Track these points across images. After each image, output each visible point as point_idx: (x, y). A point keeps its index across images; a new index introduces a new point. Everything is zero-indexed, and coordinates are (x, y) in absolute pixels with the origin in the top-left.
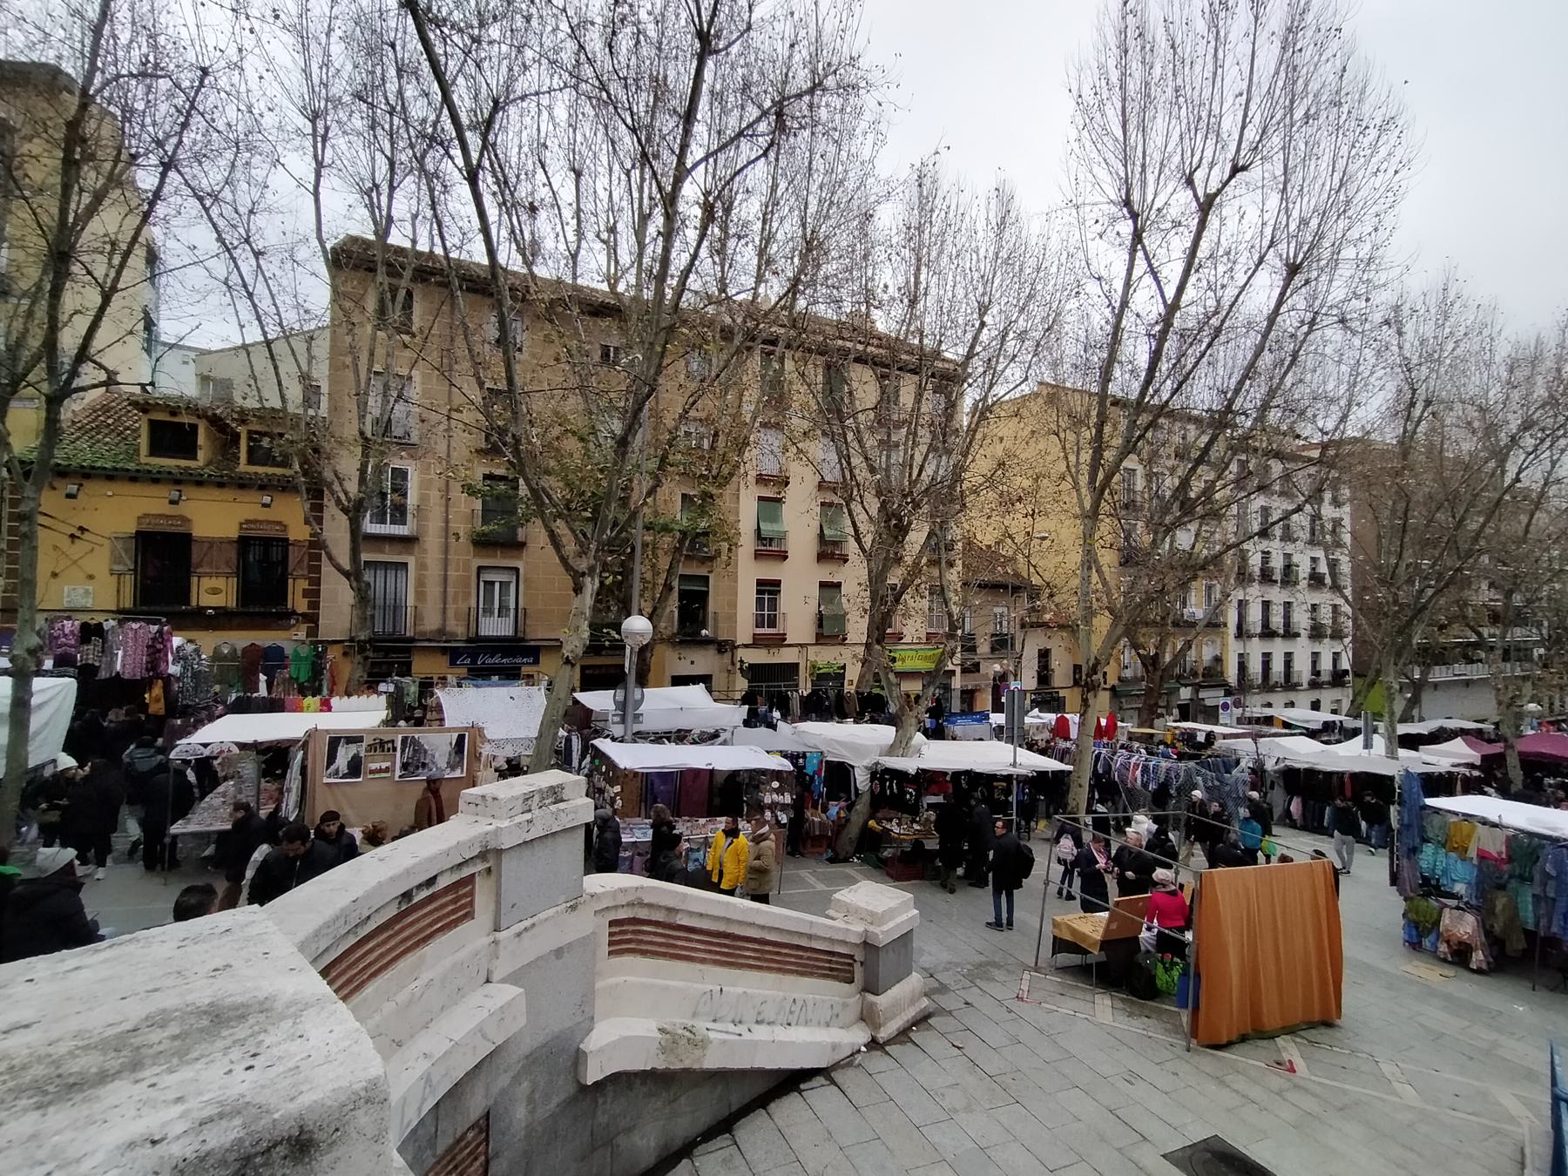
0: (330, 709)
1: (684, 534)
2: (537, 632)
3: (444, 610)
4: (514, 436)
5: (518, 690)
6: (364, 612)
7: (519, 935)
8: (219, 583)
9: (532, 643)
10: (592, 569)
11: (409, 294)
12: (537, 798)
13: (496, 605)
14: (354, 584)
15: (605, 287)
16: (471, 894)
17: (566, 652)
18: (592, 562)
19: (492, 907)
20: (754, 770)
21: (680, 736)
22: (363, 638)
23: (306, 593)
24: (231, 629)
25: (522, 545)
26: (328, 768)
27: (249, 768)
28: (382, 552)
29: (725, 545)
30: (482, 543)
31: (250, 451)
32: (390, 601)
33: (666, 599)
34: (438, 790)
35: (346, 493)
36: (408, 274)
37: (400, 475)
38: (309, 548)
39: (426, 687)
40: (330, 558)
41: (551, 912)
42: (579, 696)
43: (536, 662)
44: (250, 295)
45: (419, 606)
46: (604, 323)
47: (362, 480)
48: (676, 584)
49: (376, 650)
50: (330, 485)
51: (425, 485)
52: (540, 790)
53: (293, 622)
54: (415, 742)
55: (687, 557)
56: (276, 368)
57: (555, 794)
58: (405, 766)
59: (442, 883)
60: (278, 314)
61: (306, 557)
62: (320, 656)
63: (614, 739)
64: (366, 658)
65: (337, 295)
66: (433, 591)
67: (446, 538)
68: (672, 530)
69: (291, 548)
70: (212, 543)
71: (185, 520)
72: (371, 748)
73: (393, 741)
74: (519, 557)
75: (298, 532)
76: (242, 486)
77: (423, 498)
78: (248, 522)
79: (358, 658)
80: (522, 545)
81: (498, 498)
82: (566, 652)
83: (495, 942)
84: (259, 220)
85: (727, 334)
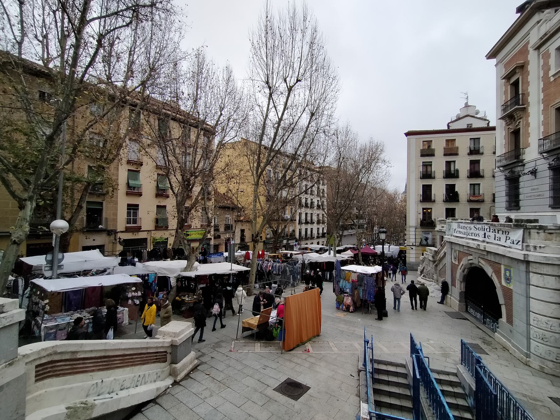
1: (89, 183)
15: (41, 63)
21: (85, 273)
29: (111, 189)
33: (79, 212)
55: (90, 193)
63: (45, 278)
68: (82, 181)
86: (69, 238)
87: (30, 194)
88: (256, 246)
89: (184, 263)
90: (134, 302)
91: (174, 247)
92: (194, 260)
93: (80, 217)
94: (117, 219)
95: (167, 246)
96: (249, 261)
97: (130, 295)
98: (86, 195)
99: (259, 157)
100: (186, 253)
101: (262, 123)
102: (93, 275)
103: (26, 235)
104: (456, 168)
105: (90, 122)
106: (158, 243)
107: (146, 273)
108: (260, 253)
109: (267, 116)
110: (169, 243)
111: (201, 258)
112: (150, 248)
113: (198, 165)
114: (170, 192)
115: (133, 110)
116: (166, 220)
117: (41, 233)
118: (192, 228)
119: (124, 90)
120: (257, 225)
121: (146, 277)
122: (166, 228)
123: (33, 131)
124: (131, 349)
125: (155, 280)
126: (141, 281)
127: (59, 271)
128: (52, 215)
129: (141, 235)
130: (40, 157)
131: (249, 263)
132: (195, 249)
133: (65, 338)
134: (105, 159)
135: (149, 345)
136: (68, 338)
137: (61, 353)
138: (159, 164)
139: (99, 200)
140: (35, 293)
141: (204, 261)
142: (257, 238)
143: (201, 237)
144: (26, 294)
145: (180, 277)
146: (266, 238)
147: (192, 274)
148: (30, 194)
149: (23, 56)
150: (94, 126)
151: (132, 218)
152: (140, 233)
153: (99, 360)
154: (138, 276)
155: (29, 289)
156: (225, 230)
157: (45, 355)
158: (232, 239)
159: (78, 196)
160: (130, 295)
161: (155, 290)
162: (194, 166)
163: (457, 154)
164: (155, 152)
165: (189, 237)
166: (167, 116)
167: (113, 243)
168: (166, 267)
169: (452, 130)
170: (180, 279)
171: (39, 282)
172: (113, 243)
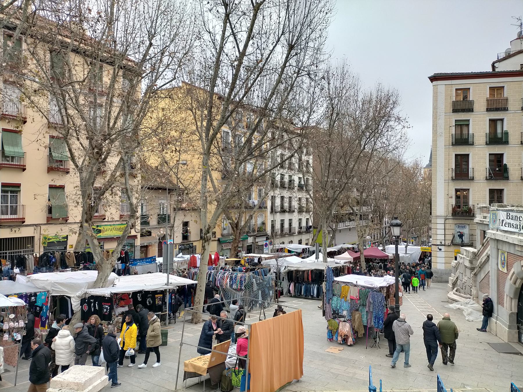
88: (206, 247)
89: (92, 275)
90: (13, 336)
91: (77, 251)
92: (109, 271)
95: (66, 248)
96: (196, 270)
100: (96, 259)
101: (214, 59)
104: (505, 129)
106: (51, 244)
107: (33, 291)
108: (213, 257)
109: (222, 48)
110: (69, 243)
111: (120, 266)
112: (39, 251)
113: (115, 123)
114: (71, 165)
116: (64, 208)
121: (33, 298)
125: (47, 302)
126: (25, 304)
129: (24, 232)
131: (195, 273)
132: (111, 252)
141: (125, 272)
142: (208, 235)
143: (119, 234)
145: (87, 296)
147: (106, 292)
152: (23, 229)
154: (20, 296)
156: (159, 223)
158: (168, 237)
162: (109, 125)
163: (506, 109)
165: (102, 235)
169: (501, 72)
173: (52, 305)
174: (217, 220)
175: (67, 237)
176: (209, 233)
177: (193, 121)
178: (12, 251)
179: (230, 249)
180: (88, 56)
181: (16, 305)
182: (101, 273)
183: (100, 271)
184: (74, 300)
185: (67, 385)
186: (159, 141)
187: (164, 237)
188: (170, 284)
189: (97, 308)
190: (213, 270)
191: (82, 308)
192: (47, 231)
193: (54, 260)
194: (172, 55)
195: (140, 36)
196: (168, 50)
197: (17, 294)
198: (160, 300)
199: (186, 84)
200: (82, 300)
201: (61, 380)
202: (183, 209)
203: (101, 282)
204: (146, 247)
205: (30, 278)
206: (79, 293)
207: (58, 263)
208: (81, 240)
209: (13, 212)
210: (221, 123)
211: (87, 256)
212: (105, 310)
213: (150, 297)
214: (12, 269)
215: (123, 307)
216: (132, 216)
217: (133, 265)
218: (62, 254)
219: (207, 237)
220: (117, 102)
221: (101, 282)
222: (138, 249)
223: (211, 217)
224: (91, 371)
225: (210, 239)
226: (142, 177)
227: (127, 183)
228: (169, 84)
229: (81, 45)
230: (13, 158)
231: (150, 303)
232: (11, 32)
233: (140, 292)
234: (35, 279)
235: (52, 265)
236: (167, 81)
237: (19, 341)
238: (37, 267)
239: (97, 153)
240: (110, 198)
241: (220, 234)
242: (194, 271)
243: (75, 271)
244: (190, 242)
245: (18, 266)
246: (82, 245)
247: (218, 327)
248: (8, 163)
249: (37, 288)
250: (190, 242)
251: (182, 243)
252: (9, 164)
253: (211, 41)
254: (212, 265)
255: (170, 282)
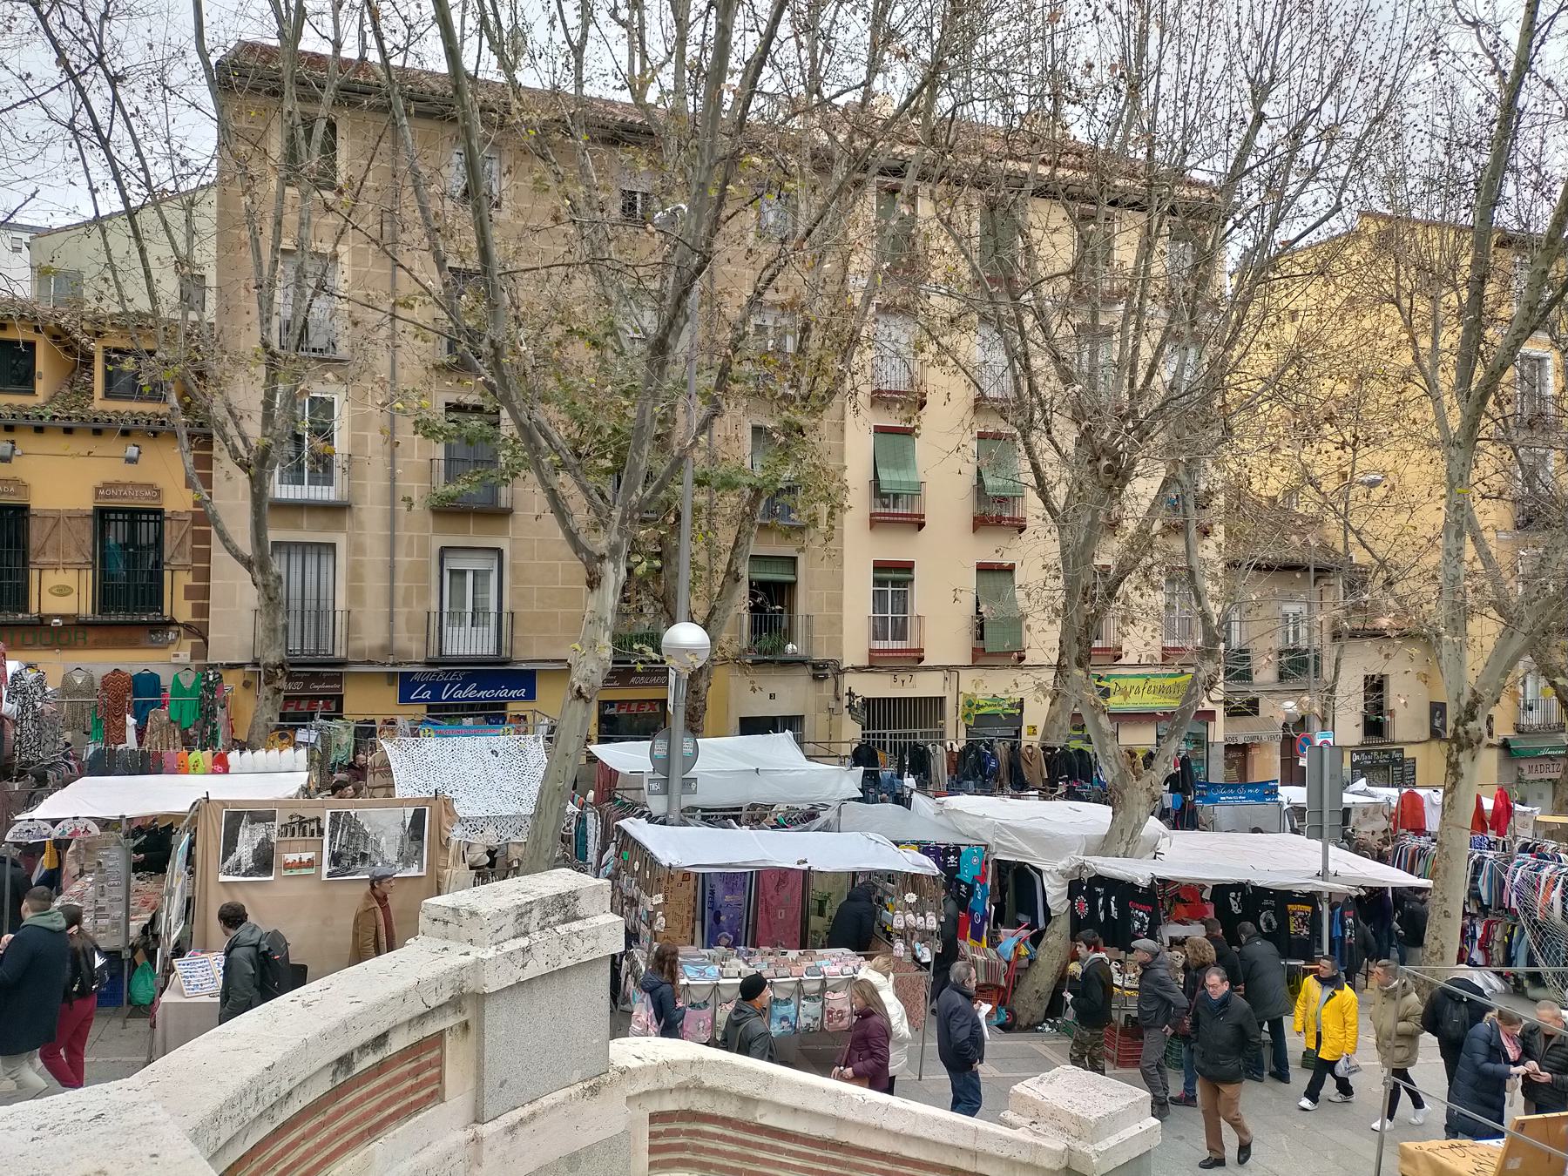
0: (226, 771)
2: (529, 650)
3: (391, 617)
4: (492, 342)
5: (502, 740)
6: (274, 620)
7: (511, 1130)
8: (68, 578)
9: (524, 667)
10: (615, 550)
11: (332, 127)
12: (536, 914)
13: (469, 608)
14: (259, 578)
16: (439, 1062)
17: (577, 680)
18: (615, 537)
19: (471, 1084)
20: (876, 873)
21: (755, 816)
22: (271, 660)
23: (189, 592)
24: (86, 646)
25: (506, 513)
26: (225, 860)
27: (116, 858)
28: (298, 527)
29: (823, 509)
30: (447, 511)
31: (109, 378)
32: (310, 604)
33: (731, 594)
34: (385, 898)
35: (245, 440)
36: (328, 95)
37: (324, 407)
38: (194, 522)
39: (365, 734)
40: (225, 540)
41: (560, 1095)
42: (599, 750)
43: (531, 696)
44: (105, 143)
45: (354, 610)
46: (624, 155)
47: (268, 418)
48: (744, 570)
49: (291, 678)
50: (221, 428)
51: (360, 422)
52: (542, 900)
53: (171, 636)
54: (352, 822)
55: (763, 527)
56: (142, 251)
57: (565, 907)
58: (336, 859)
59: (397, 1044)
60: (144, 169)
61: (189, 538)
62: (211, 688)
63: (651, 819)
64: (278, 691)
65: (226, 135)
66: (374, 585)
67: (393, 503)
68: (737, 486)
69: (167, 523)
70: (57, 519)
71: (22, 486)
72: (287, 829)
73: (318, 820)
74: (503, 533)
75: (177, 500)
76: (97, 432)
77: (357, 443)
78: (107, 485)
79: (266, 691)
80: (506, 513)
81: (469, 441)
82: (577, 680)
83: (477, 1140)
84: (116, 28)
85: (822, 162)
86: (704, 685)
87: (612, 538)
88: (1465, 768)
89: (1096, 817)
90: (914, 950)
91: (1049, 744)
92: (1142, 810)
93: (733, 612)
94: (841, 618)
95: (1018, 733)
96: (1424, 841)
97: (898, 922)
98: (750, 534)
99: (1477, 295)
100: (1107, 773)
101: (1493, 111)
102: (777, 826)
103: (605, 670)
105: (768, 266)
106: (984, 720)
107: (952, 840)
108: (1488, 804)
109: (1524, 64)
110: (1027, 721)
111: (1169, 800)
112: (956, 738)
113: (1150, 376)
114: (1032, 505)
115: (893, 191)
116: (1016, 624)
117: (639, 667)
118: (1123, 661)
119: (861, 118)
120: (1469, 656)
121: (952, 859)
122: (1017, 659)
123: (613, 332)
124: (920, 1139)
125: (985, 874)
126: (938, 871)
127: (688, 801)
128: (660, 606)
129: (924, 686)
130: (632, 414)
131: (1421, 853)
132: (1140, 756)
133: (705, 1037)
134: (805, 399)
135: (981, 1145)
136: (725, 1044)
137: (713, 1091)
138: (993, 393)
139: (787, 550)
140: (627, 866)
141: (1184, 819)
142: (1471, 725)
143: (1173, 704)
144: (606, 864)
145: (1085, 876)
146: (1519, 729)
147: (1139, 871)
148: (612, 538)
149: (588, 90)
150: (780, 281)
151: (890, 614)
152: (920, 677)
153: (819, 1153)
154: (925, 849)
155: (612, 850)
156: (1282, 676)
157: (672, 1086)
158: (1317, 725)
159: (726, 537)
160: (898, 922)
161: (985, 917)
162: (1132, 383)
164: (973, 346)
165: (1115, 702)
166: (1017, 182)
167: (831, 710)
168: (1025, 825)
170: (1084, 887)
171: (636, 827)
172: (831, 710)
173: (996, 884)
174: (1506, 674)
175: (1021, 705)
176: (1473, 718)
177: (1405, 336)
178: (897, 731)
179: (1554, 782)
180: (1073, 198)
181: (918, 871)
182: (1121, 813)
183: (1118, 809)
184: (1051, 880)
185: (1052, 1116)
186: (1295, 416)
187: (1302, 723)
188: (1331, 877)
189: (1114, 914)
190: (1490, 848)
191: (1072, 905)
192: (982, 686)
193: (993, 764)
194: (1330, 135)
195: (1232, 102)
196: (1314, 122)
197: (918, 843)
198: (1303, 923)
199: (1377, 216)
200: (1071, 884)
201: (1030, 1093)
202: (1378, 634)
203: (1119, 839)
204: (1244, 748)
205: (942, 804)
206: (1062, 864)
207: (1003, 774)
208: (1057, 715)
209: (898, 634)
210: (1521, 330)
211: (1076, 760)
212: (1137, 924)
213: (1269, 907)
214: (900, 776)
215: (1183, 923)
216: (1209, 652)
217: (1206, 799)
218: (1012, 748)
219: (1467, 733)
220: (1157, 316)
221: (1119, 839)
222: (1217, 755)
223: (1480, 665)
224: (1115, 1093)
225: (1479, 742)
226: (1229, 533)
227: (1192, 554)
228: (1315, 232)
229: (1060, 173)
230: (896, 496)
231: (1269, 925)
232: (894, 180)
233: (1239, 887)
234: (955, 810)
235: (990, 777)
236: (1311, 222)
237: (927, 965)
238: (953, 778)
239: (1109, 469)
240: (1135, 596)
241: (1511, 727)
242: (1414, 845)
243: (1045, 799)
244: (1393, 743)
245: (913, 772)
246: (1061, 729)
247: (1527, 1054)
248: (887, 511)
249: (960, 833)
250: (1393, 743)
251: (1362, 745)
252: (889, 515)
253: (1479, 50)
254: (1484, 830)
255: (1332, 868)
